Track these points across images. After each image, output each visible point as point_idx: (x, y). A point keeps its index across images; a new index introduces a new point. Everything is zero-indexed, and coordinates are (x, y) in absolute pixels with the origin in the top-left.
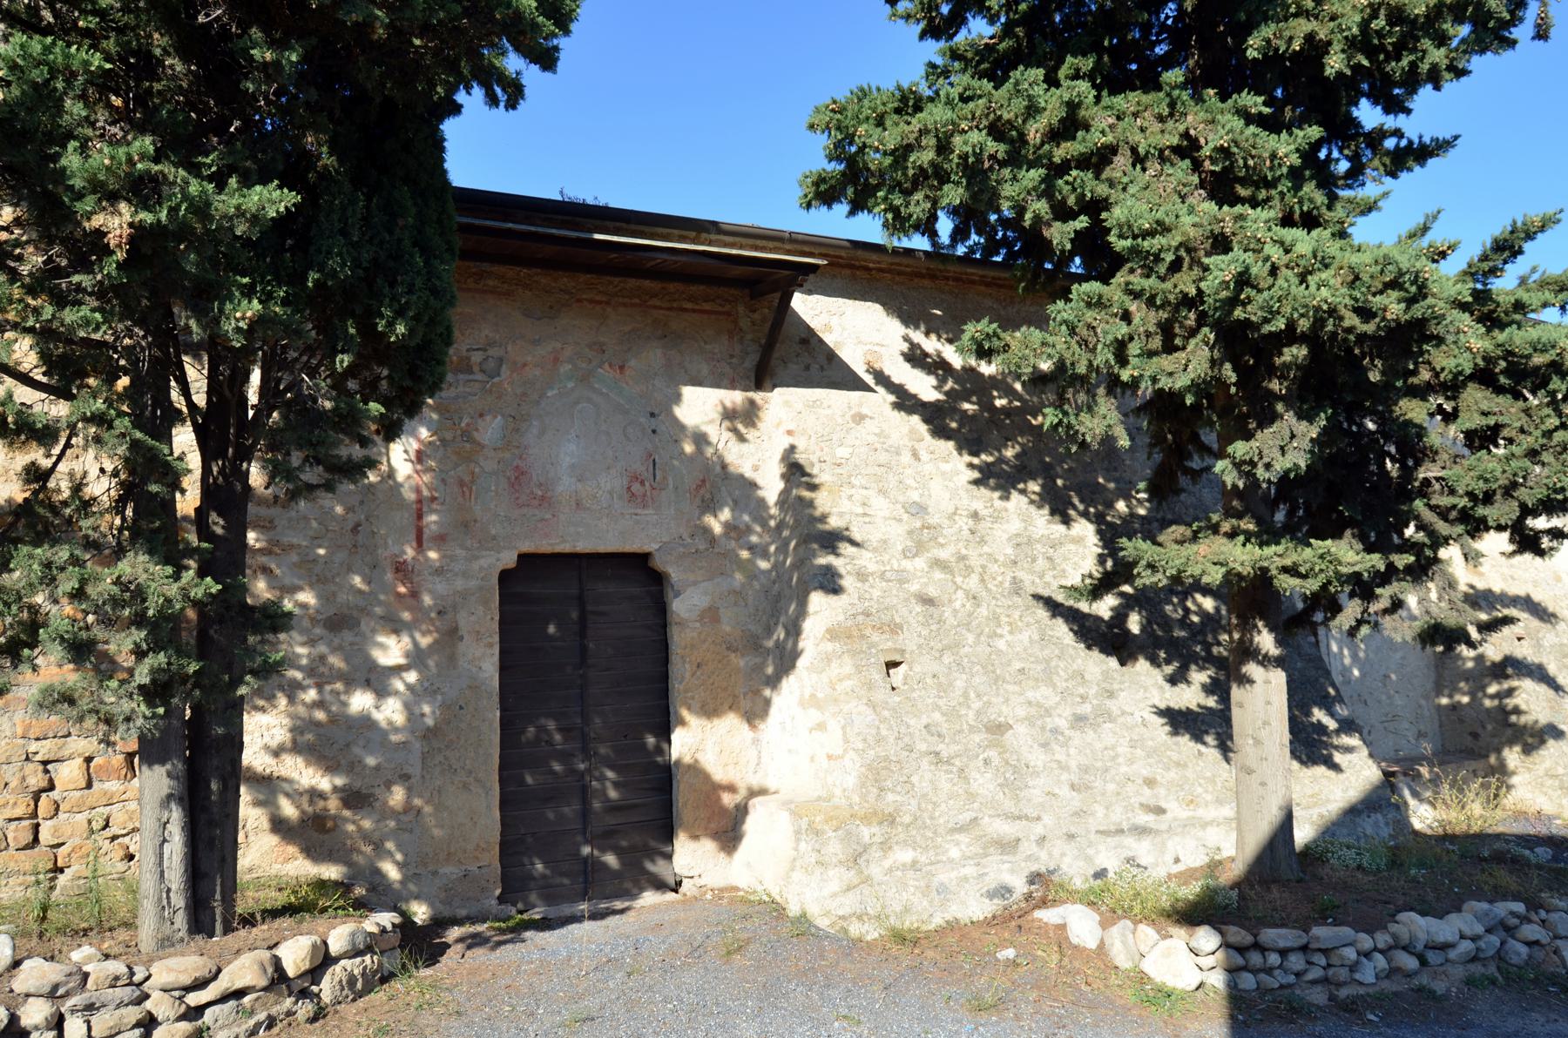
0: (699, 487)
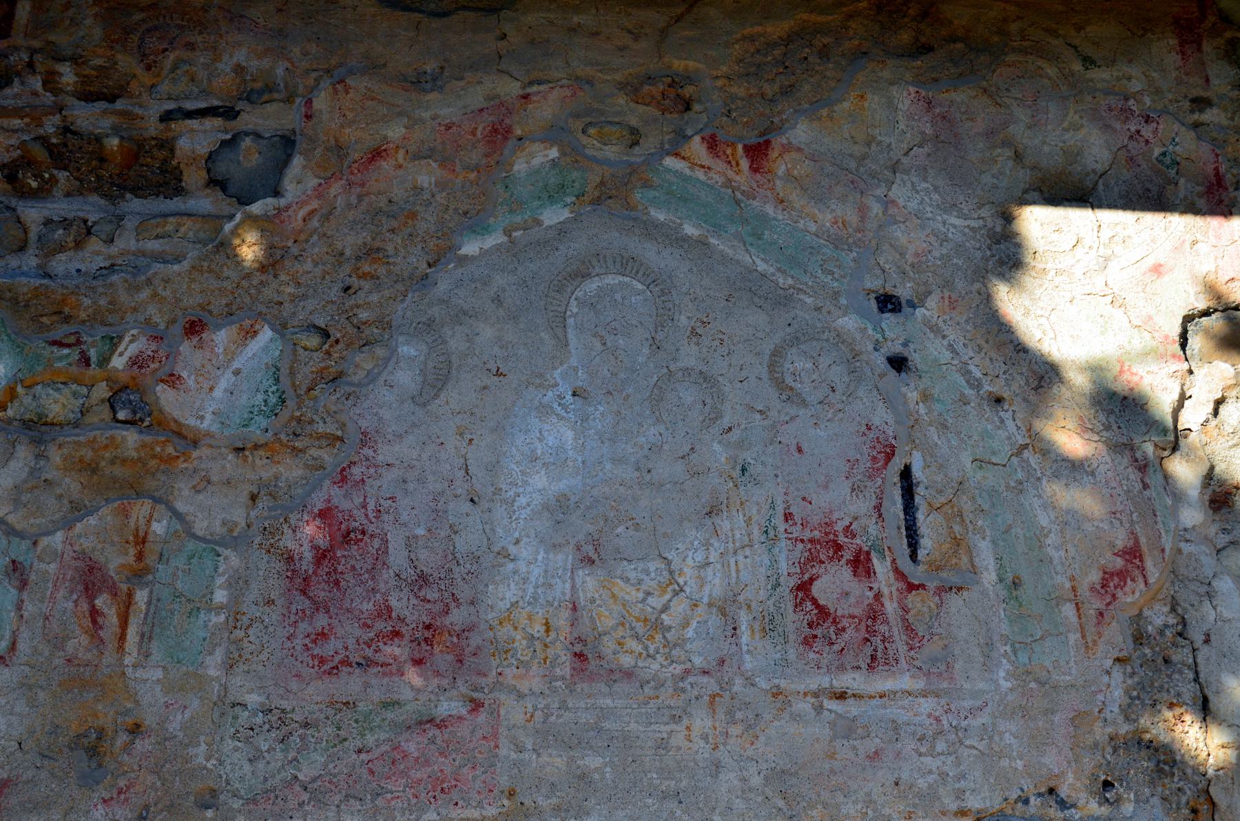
0: (1112, 581)
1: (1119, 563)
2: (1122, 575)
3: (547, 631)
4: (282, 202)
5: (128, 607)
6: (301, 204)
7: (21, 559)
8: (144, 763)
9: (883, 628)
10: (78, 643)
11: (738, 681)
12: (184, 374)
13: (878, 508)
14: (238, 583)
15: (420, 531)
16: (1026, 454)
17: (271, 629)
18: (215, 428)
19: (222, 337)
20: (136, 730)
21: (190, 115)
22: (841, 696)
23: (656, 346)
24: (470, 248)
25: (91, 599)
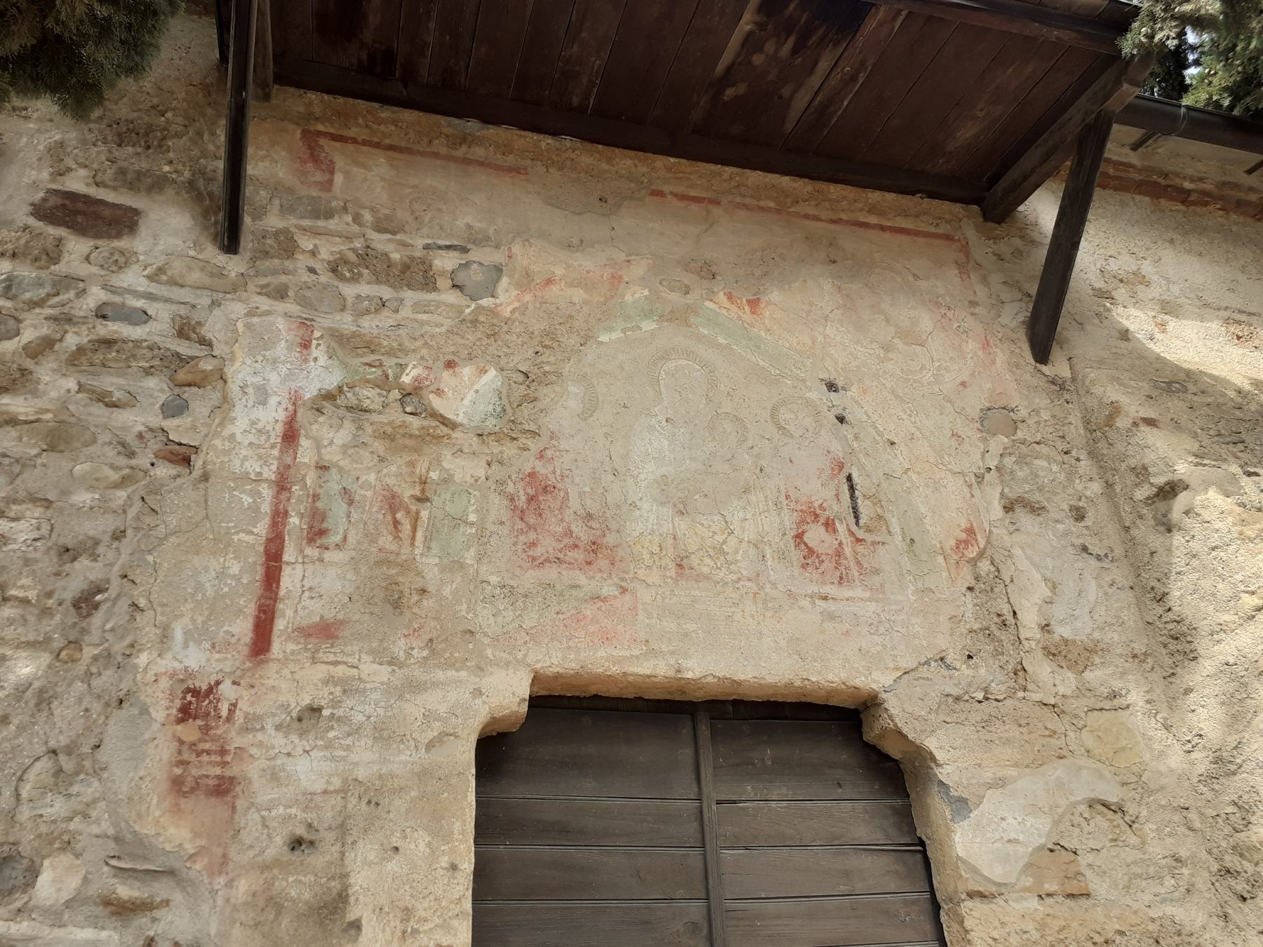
0: (961, 545)
1: (964, 536)
2: (966, 542)
3: (661, 550)
4: (498, 301)
5: (416, 520)
6: (509, 304)
7: (349, 487)
8: (429, 615)
9: (845, 562)
10: (386, 541)
11: (768, 586)
12: (446, 390)
13: (837, 495)
14: (483, 512)
15: (587, 489)
16: (910, 473)
17: (503, 539)
18: (465, 422)
19: (467, 371)
20: (423, 591)
21: (440, 248)
22: (825, 598)
23: (709, 400)
24: (604, 338)
25: (394, 515)
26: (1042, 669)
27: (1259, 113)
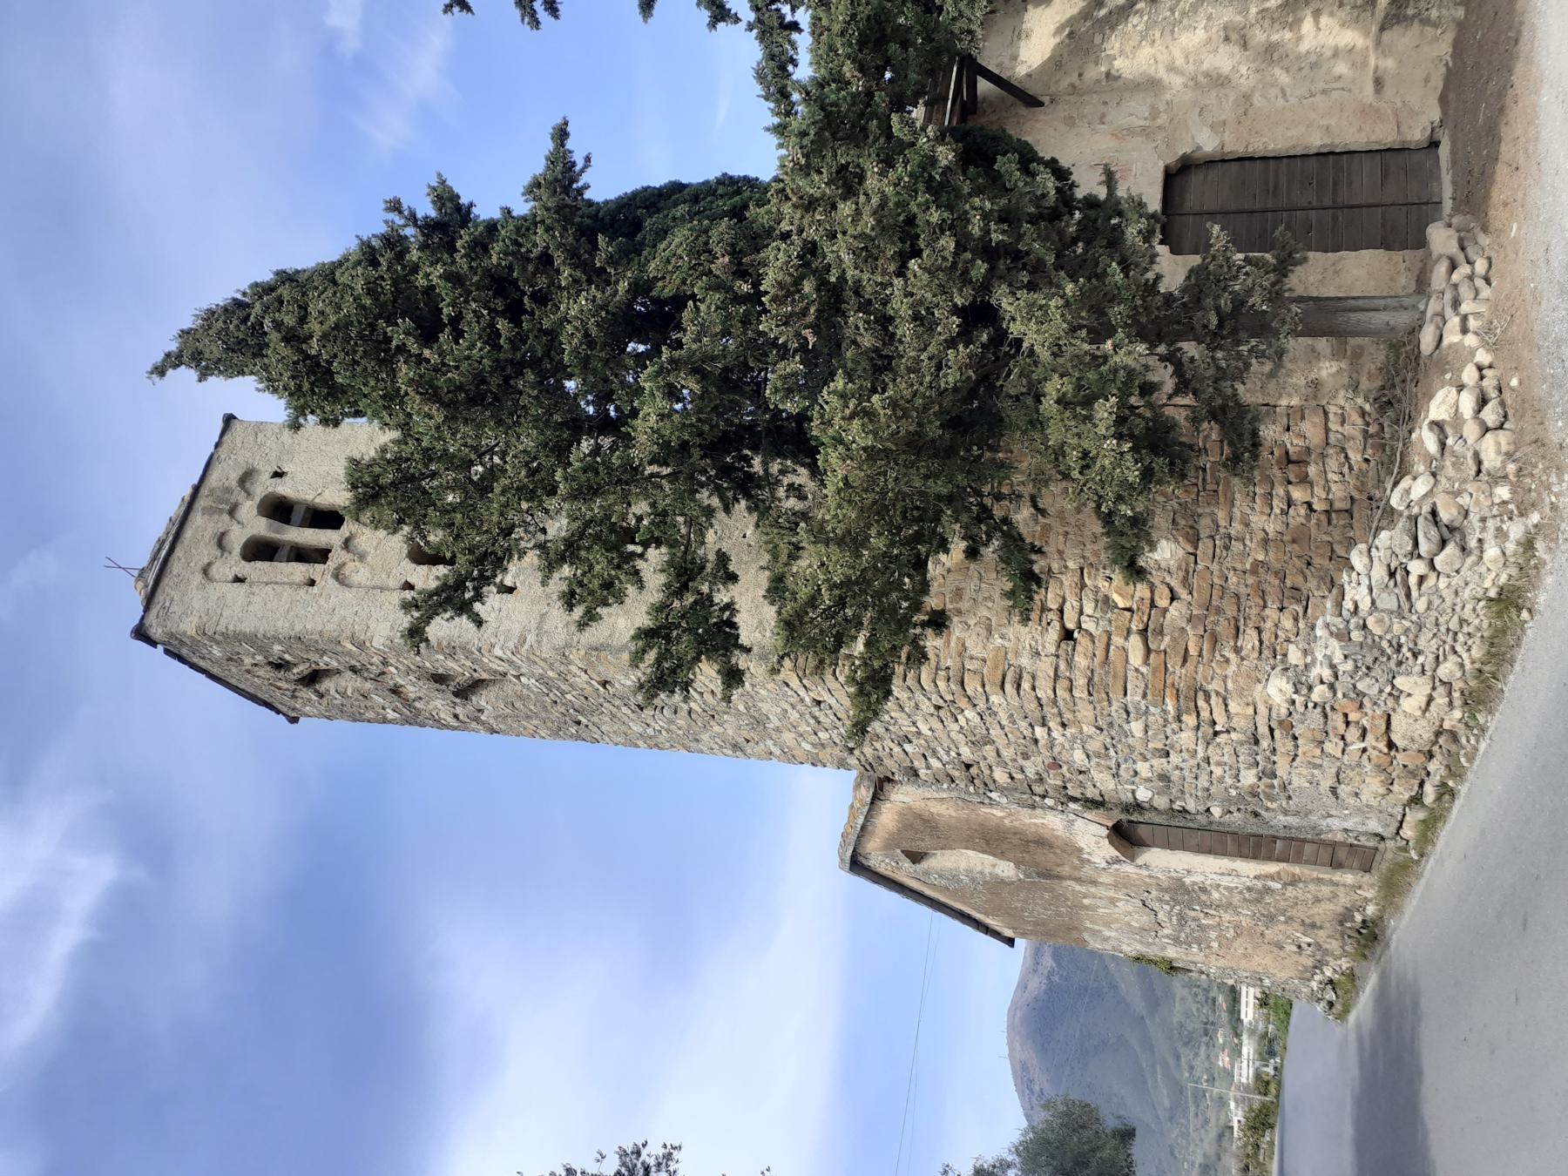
0: (1117, 137)
26: (1159, 122)
27: (545, 2)
